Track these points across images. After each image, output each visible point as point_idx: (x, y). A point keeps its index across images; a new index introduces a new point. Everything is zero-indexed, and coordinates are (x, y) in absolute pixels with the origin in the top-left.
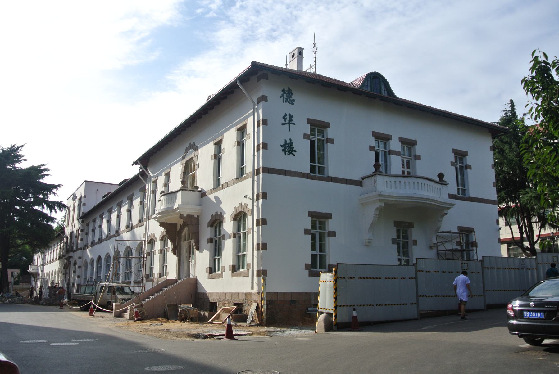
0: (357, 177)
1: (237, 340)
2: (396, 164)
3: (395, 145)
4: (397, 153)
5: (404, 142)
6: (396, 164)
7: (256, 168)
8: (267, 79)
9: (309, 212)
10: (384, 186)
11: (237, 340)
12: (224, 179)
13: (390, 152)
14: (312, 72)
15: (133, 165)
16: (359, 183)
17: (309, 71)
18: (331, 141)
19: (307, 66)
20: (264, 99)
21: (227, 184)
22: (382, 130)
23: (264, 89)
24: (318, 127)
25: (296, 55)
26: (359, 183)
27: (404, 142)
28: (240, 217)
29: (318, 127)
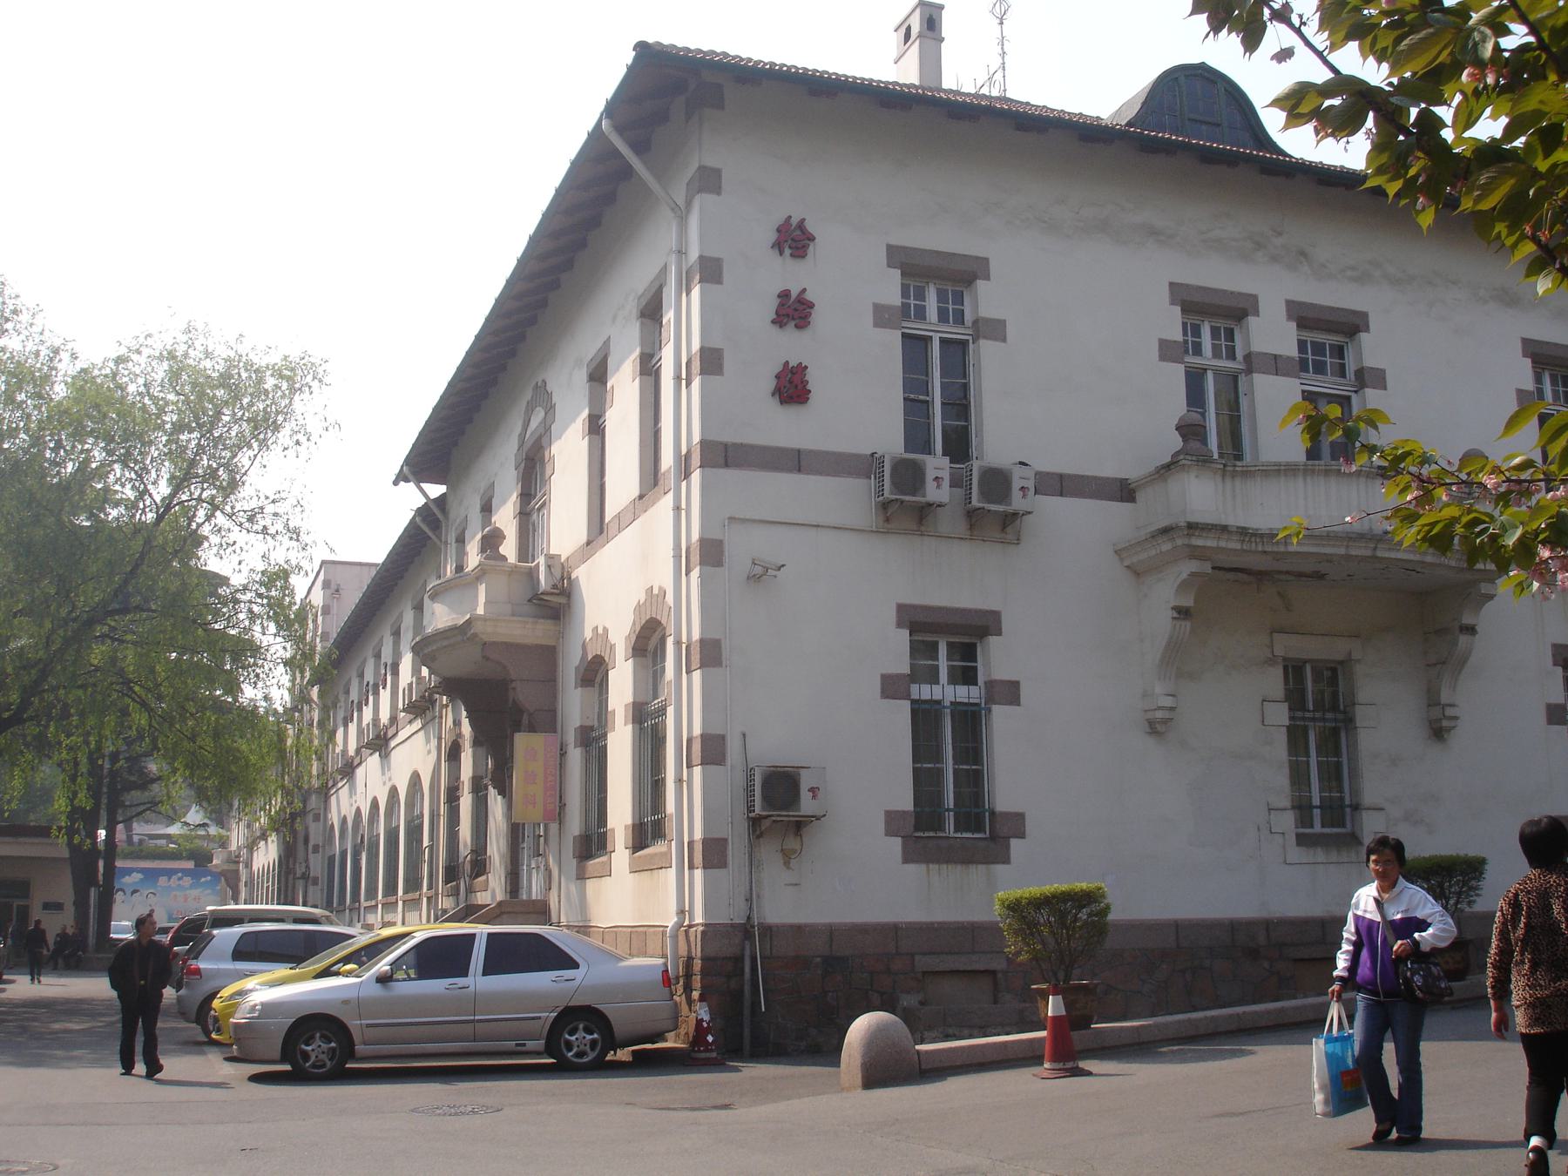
0: (1111, 469)
1: (1089, 1074)
2: (1275, 410)
3: (1271, 332)
4: (1276, 365)
5: (1305, 317)
6: (1275, 410)
7: (684, 451)
8: (719, 105)
9: (901, 608)
10: (1200, 496)
11: (1089, 1074)
12: (614, 504)
13: (1252, 363)
14: (995, 93)
15: (396, 483)
16: (1124, 491)
17: (985, 91)
18: (996, 329)
19: (963, 74)
20: (709, 181)
21: (624, 521)
22: (1219, 275)
23: (712, 148)
24: (937, 278)
25: (915, 31)
26: (1124, 491)
27: (1305, 317)
28: (648, 642)
29: (937, 278)
